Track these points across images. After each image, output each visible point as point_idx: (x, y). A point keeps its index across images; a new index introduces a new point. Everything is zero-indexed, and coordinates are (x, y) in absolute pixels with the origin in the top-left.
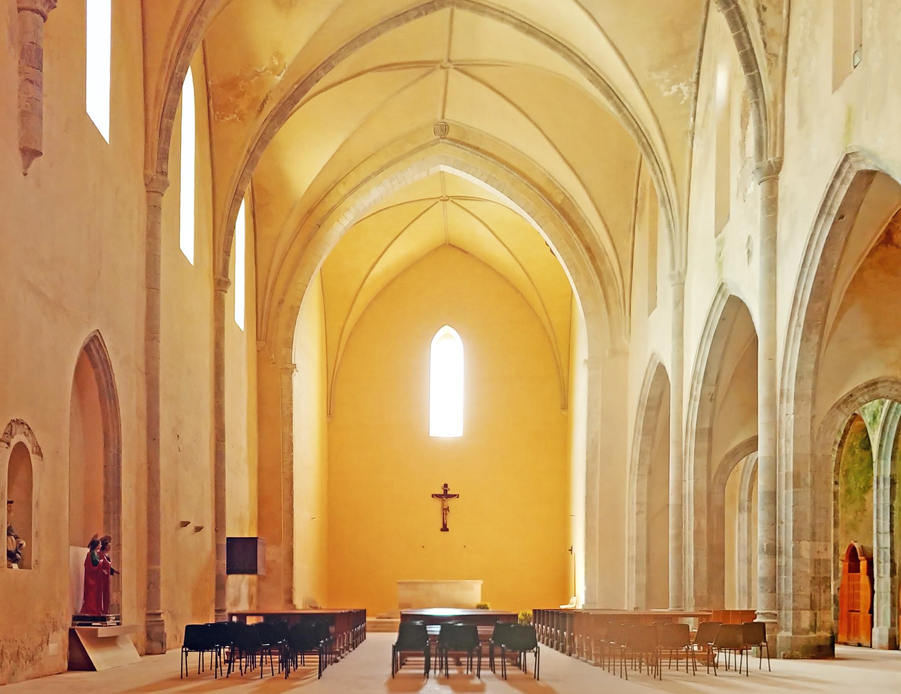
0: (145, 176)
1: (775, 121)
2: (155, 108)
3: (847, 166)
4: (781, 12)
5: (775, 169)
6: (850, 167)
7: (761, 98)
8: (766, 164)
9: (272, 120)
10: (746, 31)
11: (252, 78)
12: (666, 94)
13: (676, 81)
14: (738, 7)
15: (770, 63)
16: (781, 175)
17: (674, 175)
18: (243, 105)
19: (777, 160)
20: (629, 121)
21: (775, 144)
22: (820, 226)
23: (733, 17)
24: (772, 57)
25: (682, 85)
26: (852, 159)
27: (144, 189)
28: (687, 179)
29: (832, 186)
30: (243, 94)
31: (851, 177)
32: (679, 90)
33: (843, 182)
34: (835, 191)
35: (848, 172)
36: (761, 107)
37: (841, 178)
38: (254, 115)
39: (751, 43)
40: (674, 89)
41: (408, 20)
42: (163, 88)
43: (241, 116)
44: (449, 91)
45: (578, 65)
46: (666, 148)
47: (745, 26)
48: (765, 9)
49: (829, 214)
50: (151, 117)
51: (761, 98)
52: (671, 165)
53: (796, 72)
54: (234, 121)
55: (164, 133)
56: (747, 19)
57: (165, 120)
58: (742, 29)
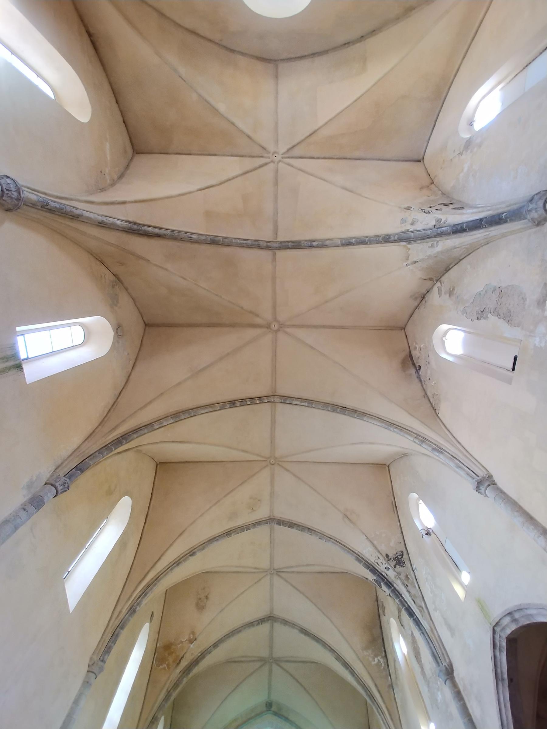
0: (91, 659)
1: (437, 640)
2: (115, 620)
3: (497, 637)
4: (415, 587)
5: (450, 670)
6: (500, 636)
7: (424, 630)
8: (444, 668)
9: (184, 673)
10: (403, 598)
11: (179, 644)
12: (373, 663)
13: (376, 656)
14: (395, 588)
15: (421, 611)
16: (455, 674)
17: (390, 714)
18: (171, 659)
19: (449, 664)
20: (360, 682)
21: (443, 654)
22: (501, 691)
23: (395, 592)
24: (420, 607)
25: (379, 658)
26: (498, 629)
27: (86, 668)
28: (397, 716)
29: (495, 657)
30: (173, 653)
31: (504, 644)
32: (378, 660)
33: (500, 651)
34: (498, 659)
35: (500, 641)
36: (425, 634)
37: (498, 648)
38: (175, 666)
39: (407, 603)
40: (376, 659)
41: (253, 626)
42: (125, 611)
43: (168, 666)
44: (253, 158)
45: (329, 651)
46: (381, 696)
47: (401, 596)
48: (407, 586)
49: (503, 680)
50: (111, 625)
51: (424, 630)
52: (387, 707)
53: (435, 609)
54: (164, 669)
55: (114, 637)
56: (401, 592)
57: (118, 629)
58: (401, 598)
